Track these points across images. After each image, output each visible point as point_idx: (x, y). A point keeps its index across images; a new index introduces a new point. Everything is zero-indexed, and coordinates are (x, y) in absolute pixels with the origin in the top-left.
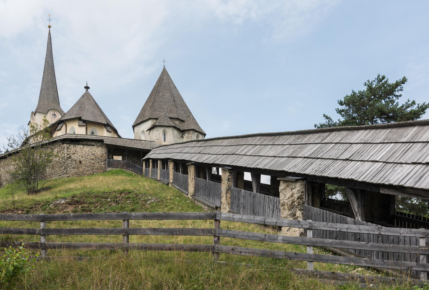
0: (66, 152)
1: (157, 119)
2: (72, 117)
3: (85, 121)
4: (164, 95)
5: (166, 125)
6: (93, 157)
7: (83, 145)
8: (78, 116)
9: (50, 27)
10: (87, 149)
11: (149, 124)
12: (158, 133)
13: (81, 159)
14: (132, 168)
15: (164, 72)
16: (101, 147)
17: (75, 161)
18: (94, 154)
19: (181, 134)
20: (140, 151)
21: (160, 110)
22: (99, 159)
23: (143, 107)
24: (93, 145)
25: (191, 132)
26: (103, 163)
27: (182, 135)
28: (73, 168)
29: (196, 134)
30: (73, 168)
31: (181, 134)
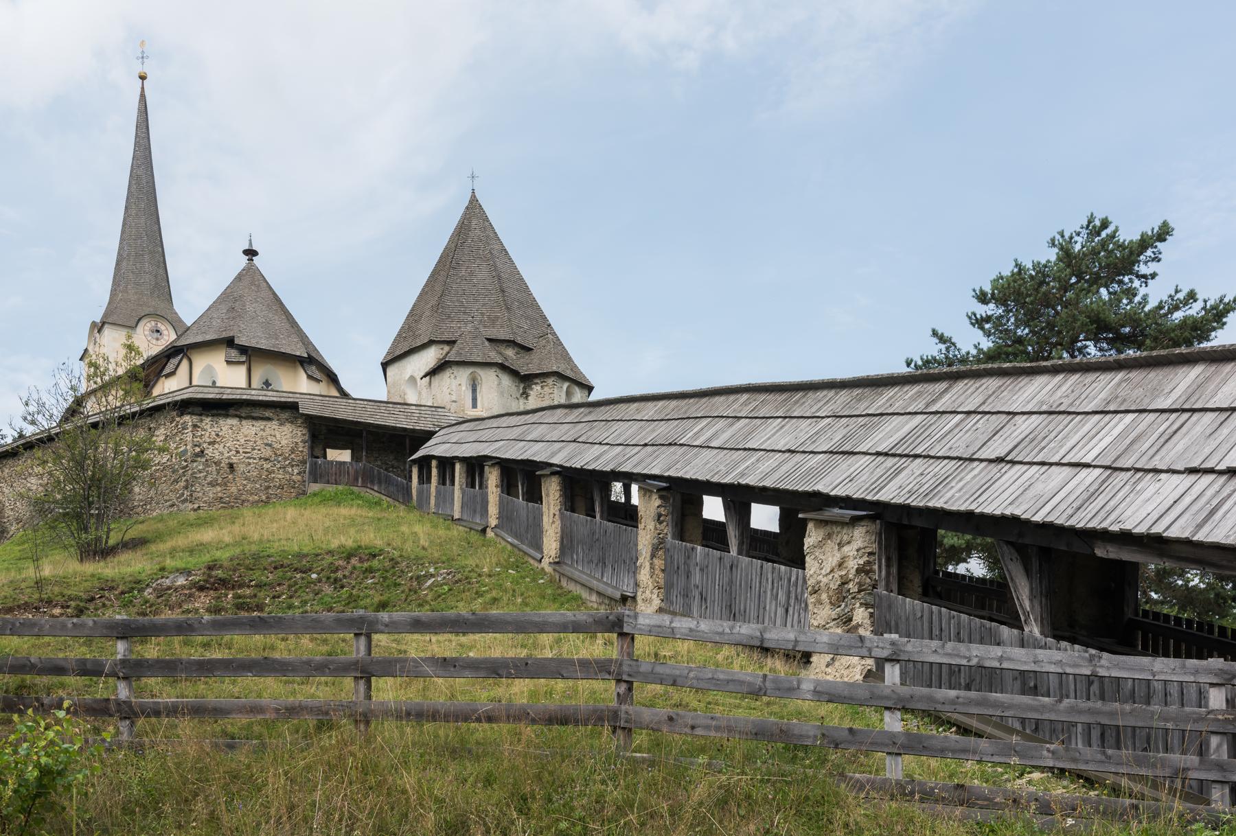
0: (189, 437)
1: (451, 343)
2: (208, 337)
3: (244, 350)
4: (471, 274)
5: (479, 359)
6: (268, 452)
7: (240, 418)
8: (224, 335)
9: (143, 78)
10: (250, 429)
11: (429, 358)
12: (455, 383)
13: (234, 460)
14: (380, 483)
15: (474, 209)
16: (292, 422)
17: (217, 463)
18: (270, 445)
19: (522, 386)
20: (404, 436)
21: (462, 316)
22: (286, 459)
23: (412, 310)
24: (269, 419)
25: (550, 381)
26: (296, 471)
27: (524, 388)
28: (211, 484)
29: (566, 385)
30: (211, 484)
31: (522, 386)
